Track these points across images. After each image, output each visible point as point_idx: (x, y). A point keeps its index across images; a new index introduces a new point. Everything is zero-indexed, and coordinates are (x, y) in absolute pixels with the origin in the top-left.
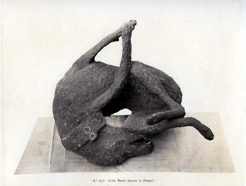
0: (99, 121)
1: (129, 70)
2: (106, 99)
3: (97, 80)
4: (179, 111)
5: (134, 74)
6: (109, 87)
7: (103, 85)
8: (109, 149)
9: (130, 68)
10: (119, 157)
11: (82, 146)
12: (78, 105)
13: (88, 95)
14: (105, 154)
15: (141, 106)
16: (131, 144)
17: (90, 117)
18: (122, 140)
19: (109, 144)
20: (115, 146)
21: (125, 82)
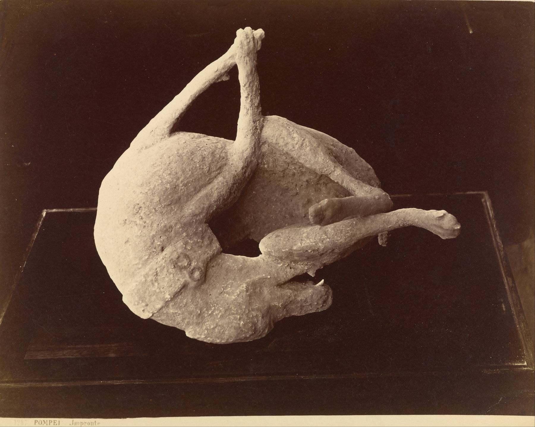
0: (206, 243)
1: (259, 135)
2: (215, 195)
3: (192, 160)
4: (377, 197)
5: (270, 141)
6: (219, 174)
7: (206, 169)
8: (234, 300)
9: (261, 130)
10: (257, 316)
11: (174, 296)
12: (156, 211)
13: (175, 188)
14: (226, 311)
15: (291, 216)
16: (280, 285)
17: (184, 234)
18: (260, 279)
19: (260, 132)
20: (247, 291)
21: (251, 161)
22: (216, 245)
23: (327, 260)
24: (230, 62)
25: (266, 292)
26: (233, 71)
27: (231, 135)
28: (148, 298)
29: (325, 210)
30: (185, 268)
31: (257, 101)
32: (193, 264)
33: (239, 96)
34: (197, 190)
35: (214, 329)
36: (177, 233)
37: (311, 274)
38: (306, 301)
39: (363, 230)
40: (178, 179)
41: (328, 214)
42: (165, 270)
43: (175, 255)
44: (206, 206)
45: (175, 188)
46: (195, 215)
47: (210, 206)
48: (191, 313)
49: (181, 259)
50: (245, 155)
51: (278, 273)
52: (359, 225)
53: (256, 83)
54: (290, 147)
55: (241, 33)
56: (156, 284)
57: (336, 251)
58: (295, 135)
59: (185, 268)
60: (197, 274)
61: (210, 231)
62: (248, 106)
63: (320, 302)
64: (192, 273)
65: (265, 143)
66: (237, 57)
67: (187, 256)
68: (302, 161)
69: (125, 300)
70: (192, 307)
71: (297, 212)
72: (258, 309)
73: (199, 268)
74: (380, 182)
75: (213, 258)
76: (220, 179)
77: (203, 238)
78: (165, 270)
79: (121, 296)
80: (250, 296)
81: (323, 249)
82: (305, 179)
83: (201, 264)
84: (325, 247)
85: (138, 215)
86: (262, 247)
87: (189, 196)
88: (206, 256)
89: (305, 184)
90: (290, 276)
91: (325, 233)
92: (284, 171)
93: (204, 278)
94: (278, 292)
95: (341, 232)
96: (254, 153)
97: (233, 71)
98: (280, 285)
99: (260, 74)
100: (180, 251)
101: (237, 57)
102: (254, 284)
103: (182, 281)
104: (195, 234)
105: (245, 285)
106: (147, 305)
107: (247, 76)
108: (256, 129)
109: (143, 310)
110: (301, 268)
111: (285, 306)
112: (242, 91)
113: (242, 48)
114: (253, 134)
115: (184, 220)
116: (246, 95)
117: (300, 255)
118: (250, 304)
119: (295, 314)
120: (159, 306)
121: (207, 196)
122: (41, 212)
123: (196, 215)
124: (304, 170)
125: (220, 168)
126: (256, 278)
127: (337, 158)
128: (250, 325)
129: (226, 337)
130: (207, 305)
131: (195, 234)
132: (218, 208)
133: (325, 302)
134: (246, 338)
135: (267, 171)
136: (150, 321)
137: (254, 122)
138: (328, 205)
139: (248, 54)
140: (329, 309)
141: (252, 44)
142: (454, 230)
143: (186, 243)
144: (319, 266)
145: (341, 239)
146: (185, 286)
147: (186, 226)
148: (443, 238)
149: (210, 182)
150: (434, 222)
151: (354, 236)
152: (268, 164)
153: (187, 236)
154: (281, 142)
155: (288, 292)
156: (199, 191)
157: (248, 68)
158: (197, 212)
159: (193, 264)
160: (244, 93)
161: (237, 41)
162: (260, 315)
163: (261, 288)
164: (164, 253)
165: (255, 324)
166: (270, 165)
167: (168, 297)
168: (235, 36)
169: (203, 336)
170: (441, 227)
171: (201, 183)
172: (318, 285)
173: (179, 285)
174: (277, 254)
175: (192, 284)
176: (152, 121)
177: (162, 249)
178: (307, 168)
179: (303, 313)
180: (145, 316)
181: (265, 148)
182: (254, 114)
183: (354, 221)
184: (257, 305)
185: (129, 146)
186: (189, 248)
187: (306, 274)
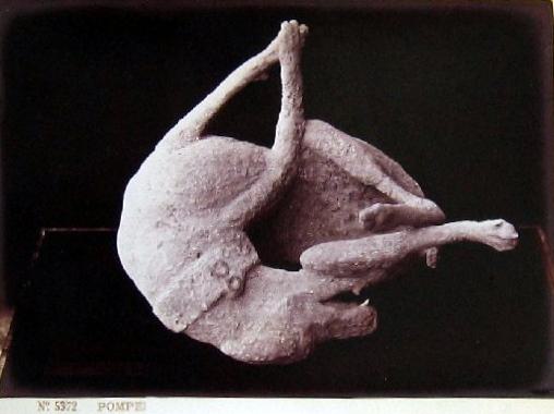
0: (244, 252)
1: (301, 139)
2: (254, 201)
14: (266, 325)
16: (323, 302)
22: (255, 256)
23: (372, 277)
24: (271, 59)
25: (308, 306)
26: (273, 69)
27: (268, 141)
28: (183, 308)
29: (377, 215)
30: (223, 276)
31: (299, 101)
32: (232, 273)
33: (280, 96)
34: (235, 195)
35: (253, 344)
36: (215, 240)
37: (356, 291)
38: (350, 321)
39: (415, 242)
40: (215, 181)
41: (380, 219)
42: (202, 278)
43: (212, 262)
44: (244, 212)
45: (211, 191)
46: (233, 221)
47: (249, 213)
48: (228, 326)
49: (219, 266)
50: (285, 161)
51: (321, 288)
52: (411, 237)
53: (300, 80)
54: (335, 153)
55: (284, 25)
56: (192, 293)
57: (385, 266)
58: (340, 140)
59: (223, 276)
60: (236, 284)
61: (248, 240)
62: (290, 106)
63: (365, 323)
64: (230, 281)
65: (306, 149)
66: (280, 52)
67: (224, 264)
68: (346, 169)
69: (156, 311)
70: (230, 319)
71: (338, 229)
72: (300, 326)
73: (238, 278)
74: (308, 351)
75: (252, 268)
76: (259, 184)
77: (241, 247)
78: (202, 278)
79: (151, 308)
80: (291, 311)
81: (371, 263)
82: (347, 191)
83: (240, 274)
84: (373, 261)
85: (172, 218)
86: (306, 257)
87: (226, 201)
88: (245, 265)
89: (347, 198)
90: (333, 292)
91: (375, 245)
92: (324, 183)
93: (241, 293)
94: (322, 308)
95: (391, 244)
96: (294, 159)
97: (273, 69)
98: (323, 302)
99: (303, 73)
100: (218, 258)
101: (280, 52)
102: (295, 298)
103: (220, 290)
104: (234, 240)
105: (286, 300)
106: (181, 316)
107: (291, 73)
108: (298, 131)
109: (177, 322)
110: (345, 284)
111: (328, 325)
112: (284, 90)
113: (287, 42)
114: (294, 139)
115: (223, 226)
116: (288, 94)
117: (345, 269)
118: (292, 319)
119: (338, 336)
120: (194, 317)
121: (246, 201)
122: (40, 231)
123: (235, 221)
124: (347, 181)
125: (258, 174)
126: (298, 292)
127: (384, 170)
128: (291, 342)
129: (265, 354)
130: (246, 318)
131: (234, 240)
132: (257, 214)
133: (370, 324)
134: (286, 357)
135: (307, 183)
136: (182, 335)
137: (296, 124)
138: (380, 210)
139: (293, 49)
140: (375, 332)
141: (297, 38)
142: (513, 240)
143: (224, 251)
144: (364, 283)
145: (390, 252)
146: (223, 296)
147: (226, 230)
148: (500, 250)
149: (248, 187)
150: (490, 232)
151: (405, 247)
152: (308, 173)
153: (225, 242)
154: (325, 147)
155: (331, 309)
156: (238, 195)
157: (292, 66)
158: (235, 218)
159: (232, 273)
160: (285, 93)
161: (281, 34)
162: (302, 333)
163: (303, 303)
164: (202, 258)
165: (296, 342)
166: (311, 175)
167: (205, 306)
168: (279, 29)
169: (241, 352)
170: (499, 237)
171: (239, 187)
172: (363, 305)
173: (216, 294)
174: (320, 268)
175: (231, 294)
176: (181, 122)
177: (198, 256)
178: (352, 178)
179: (346, 336)
180: (178, 328)
181: (306, 156)
182: (296, 116)
183: (404, 233)
184: (298, 322)
185: (153, 150)
186: (227, 255)
187: (350, 292)
